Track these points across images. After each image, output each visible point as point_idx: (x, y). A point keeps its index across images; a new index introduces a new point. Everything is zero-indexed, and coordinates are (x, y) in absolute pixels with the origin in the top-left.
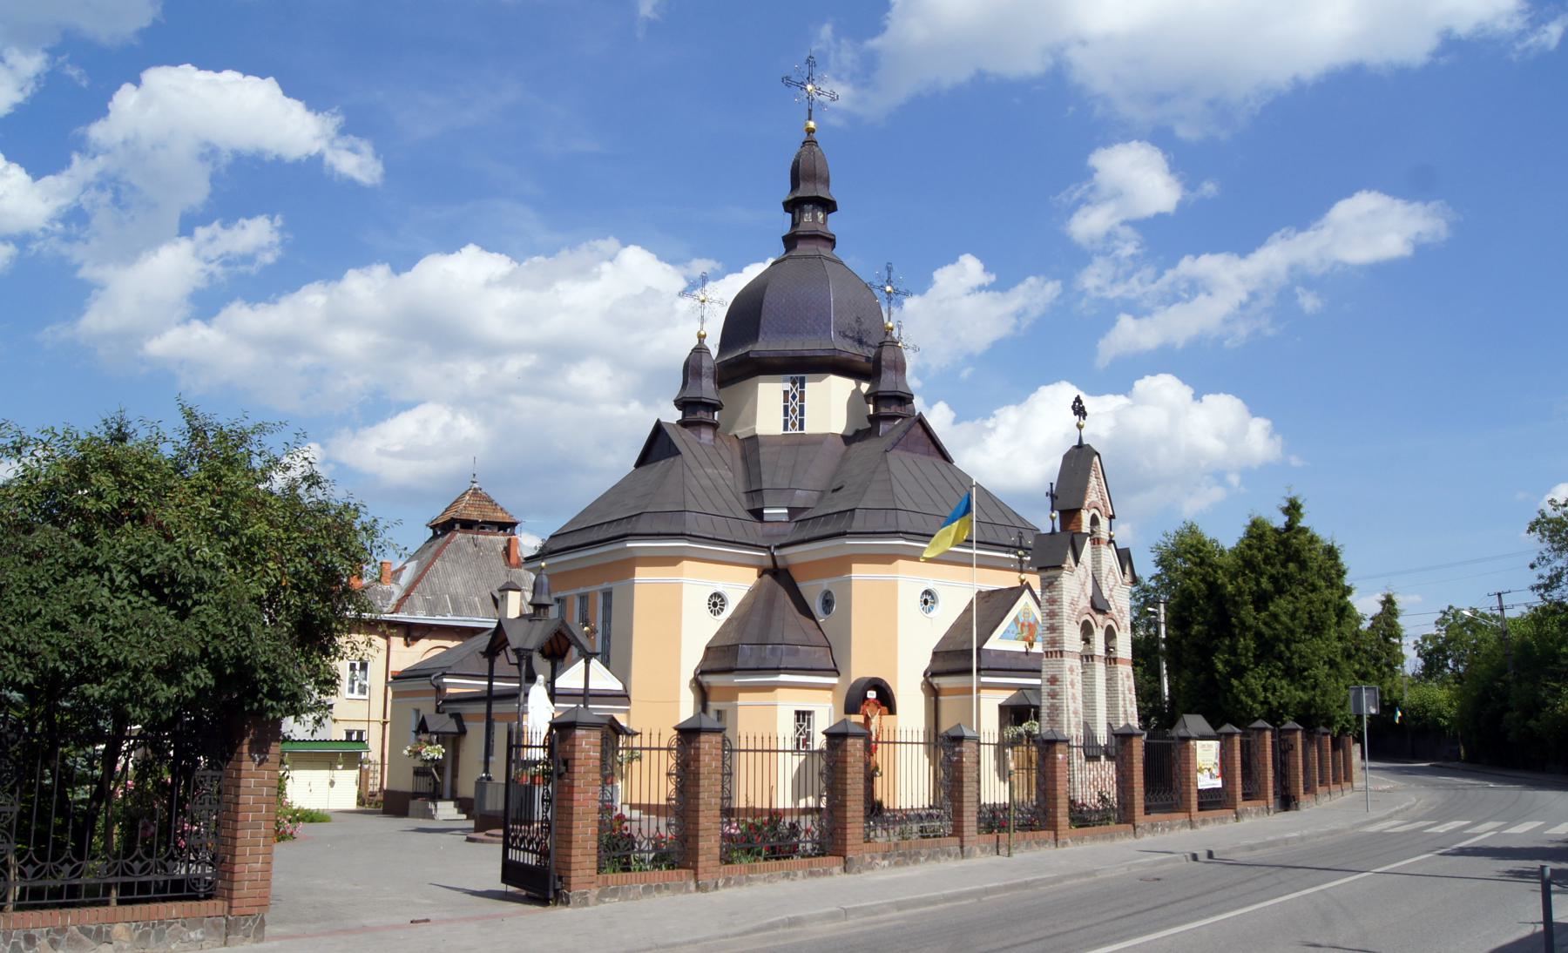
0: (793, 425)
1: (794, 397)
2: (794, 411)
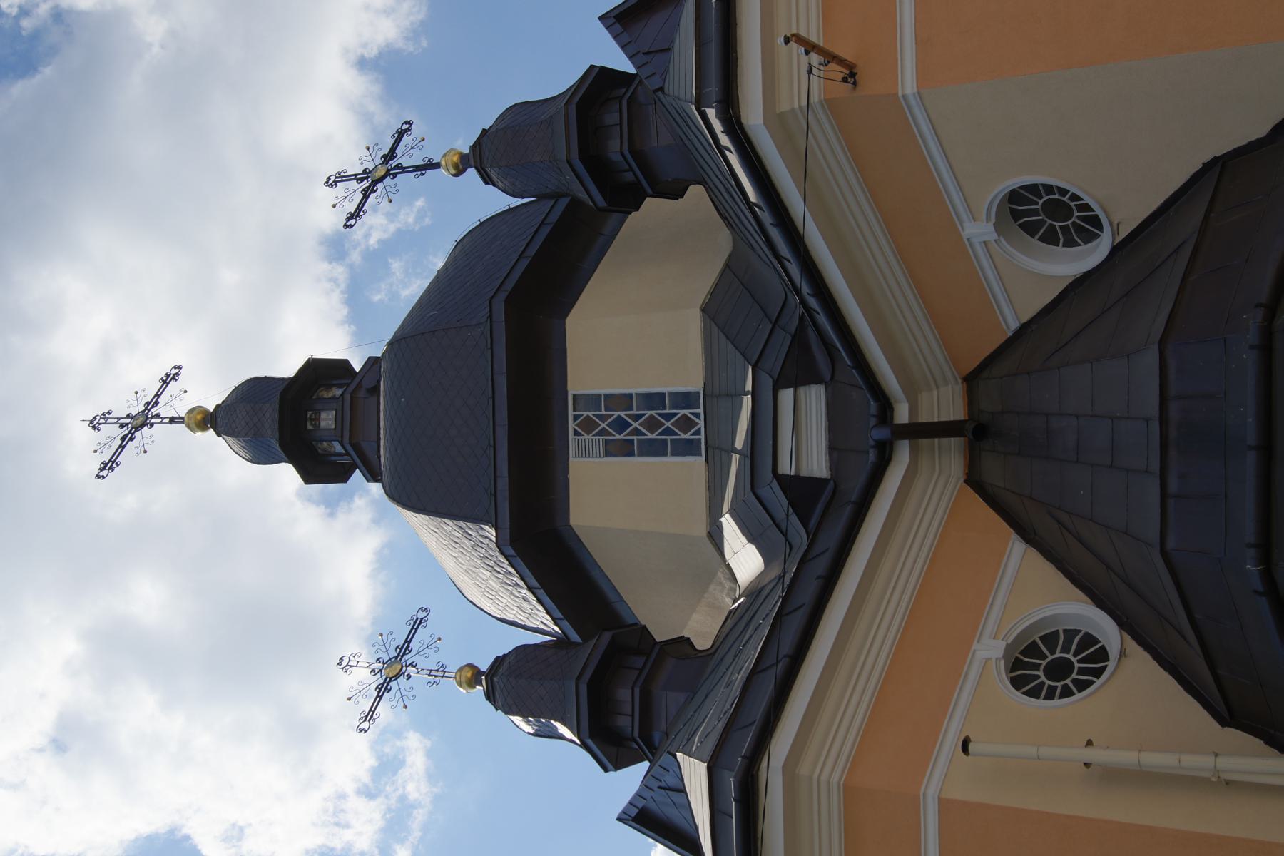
0: (686, 424)
1: (652, 424)
2: (652, 424)
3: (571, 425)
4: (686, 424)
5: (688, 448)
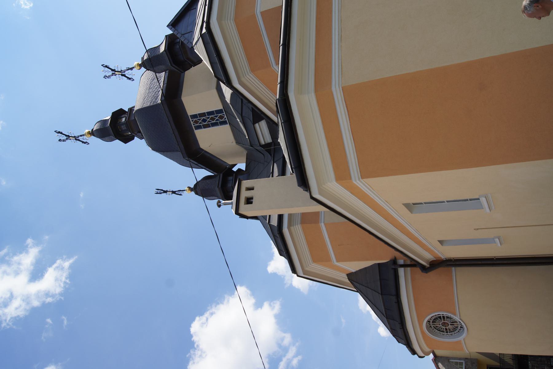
0: (221, 117)
3: (192, 123)
4: (221, 117)
5: (224, 123)
